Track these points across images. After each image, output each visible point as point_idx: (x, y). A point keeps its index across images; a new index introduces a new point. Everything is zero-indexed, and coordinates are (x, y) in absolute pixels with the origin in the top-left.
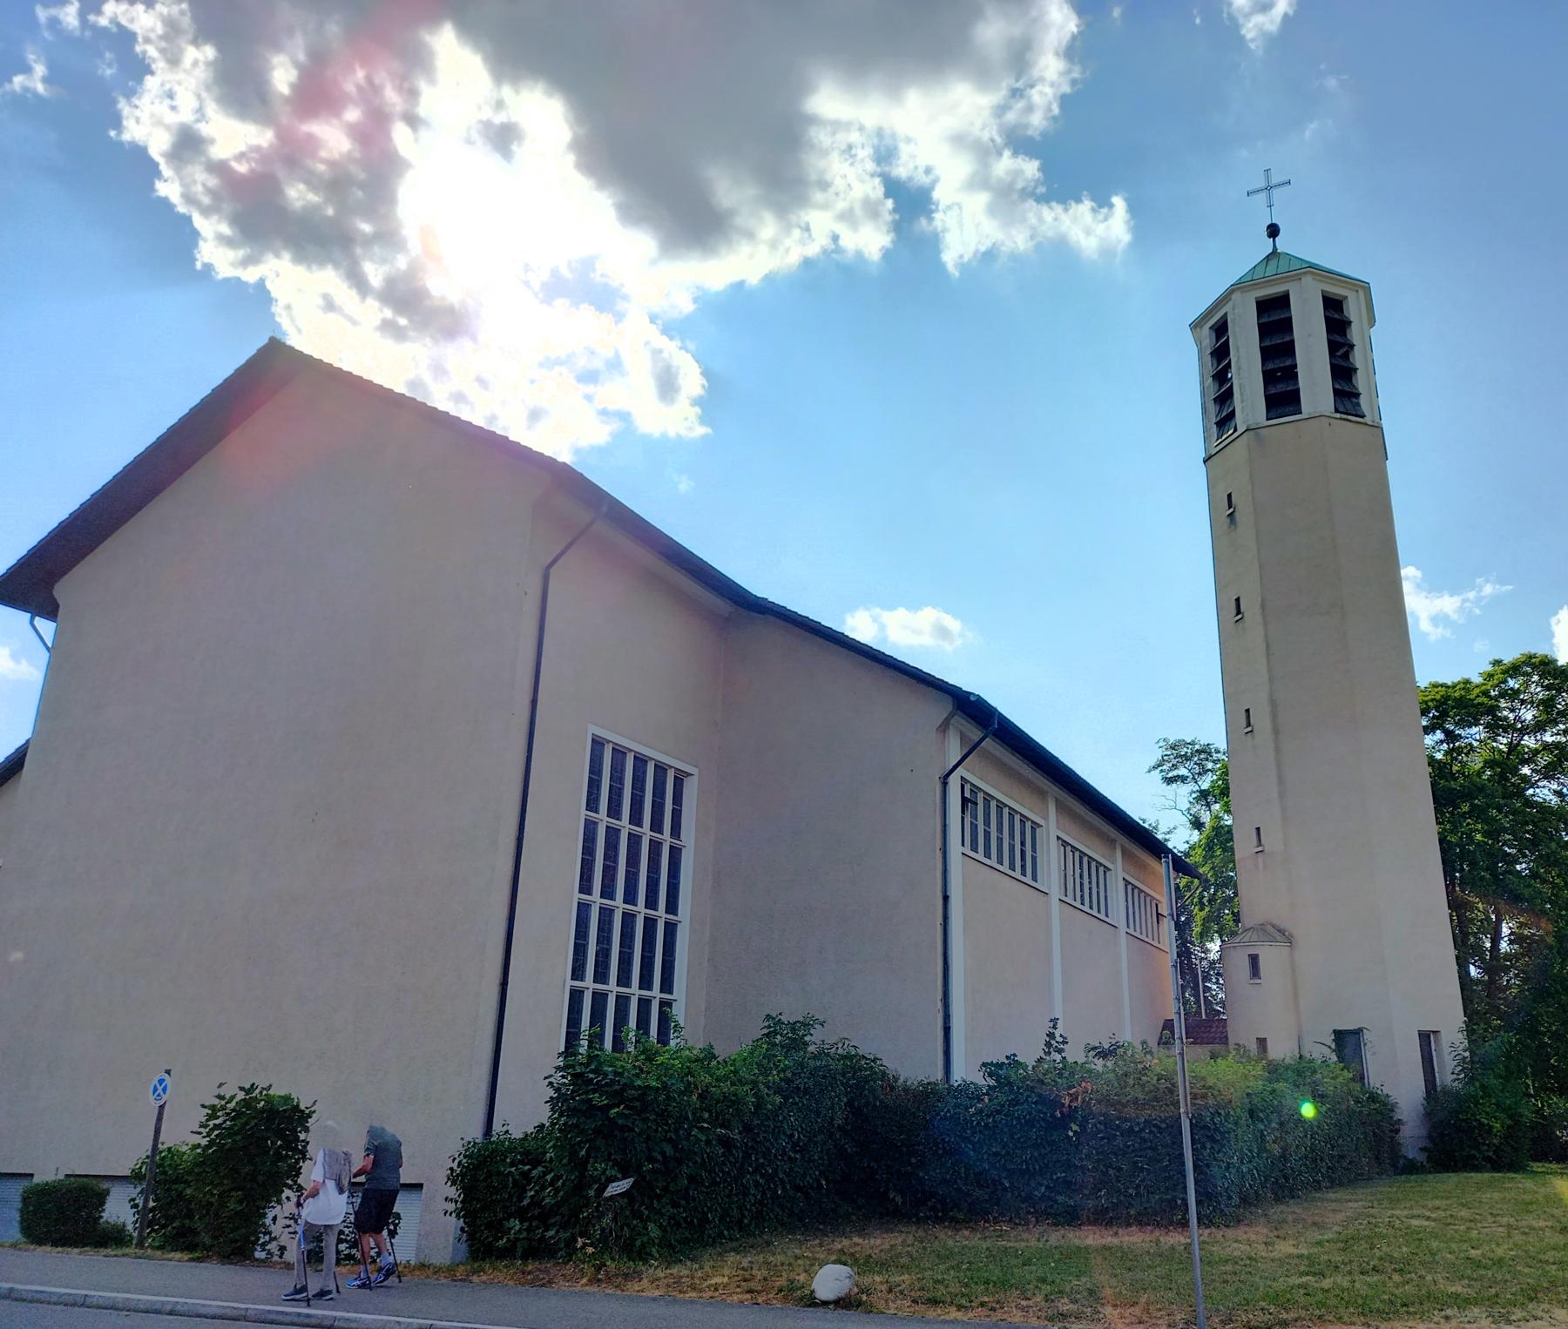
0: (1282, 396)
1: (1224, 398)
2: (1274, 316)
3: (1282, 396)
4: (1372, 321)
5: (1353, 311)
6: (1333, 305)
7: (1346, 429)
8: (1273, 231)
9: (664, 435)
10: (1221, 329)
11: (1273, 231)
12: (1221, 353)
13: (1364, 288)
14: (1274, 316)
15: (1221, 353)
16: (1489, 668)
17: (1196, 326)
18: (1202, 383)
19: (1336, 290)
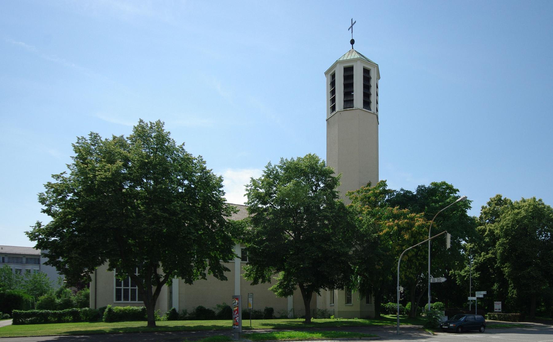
0: (349, 101)
1: (333, 100)
2: (349, 72)
3: (349, 101)
4: (379, 77)
5: (373, 74)
6: (366, 72)
7: (365, 113)
8: (352, 42)
9: (299, 159)
10: (333, 76)
11: (352, 42)
12: (333, 84)
13: (377, 66)
14: (349, 72)
15: (333, 84)
16: (162, 122)
17: (326, 73)
18: (327, 87)
19: (368, 67)
